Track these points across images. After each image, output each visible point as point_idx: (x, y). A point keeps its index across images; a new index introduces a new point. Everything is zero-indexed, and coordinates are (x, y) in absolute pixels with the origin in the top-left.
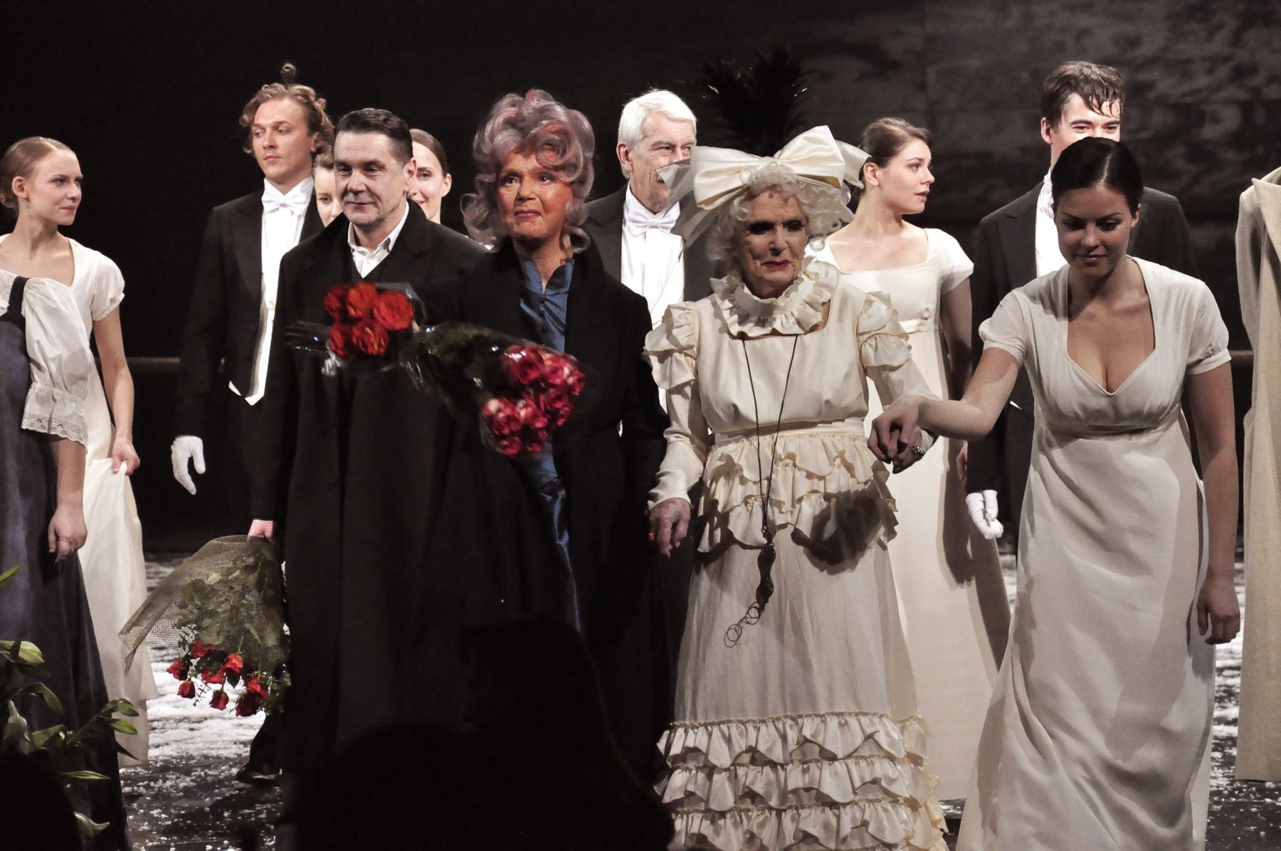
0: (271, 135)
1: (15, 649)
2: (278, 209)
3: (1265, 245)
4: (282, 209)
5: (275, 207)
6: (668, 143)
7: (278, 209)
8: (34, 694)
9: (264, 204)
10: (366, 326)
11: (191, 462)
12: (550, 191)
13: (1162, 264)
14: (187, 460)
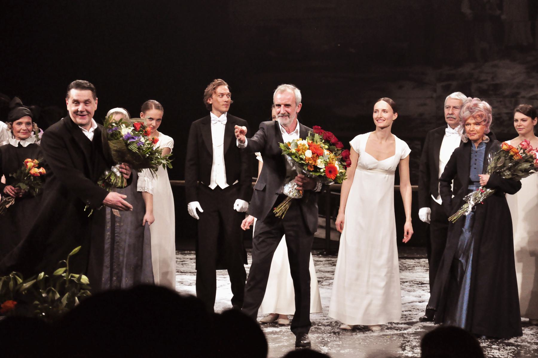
0: (381, 113)
1: (80, 278)
2: (217, 122)
3: (469, 221)
4: (218, 122)
5: (216, 122)
6: (448, 106)
7: (217, 122)
8: (85, 295)
9: (446, 132)
10: (49, 174)
11: (197, 209)
12: (478, 128)
13: (364, 133)
14: (195, 209)
